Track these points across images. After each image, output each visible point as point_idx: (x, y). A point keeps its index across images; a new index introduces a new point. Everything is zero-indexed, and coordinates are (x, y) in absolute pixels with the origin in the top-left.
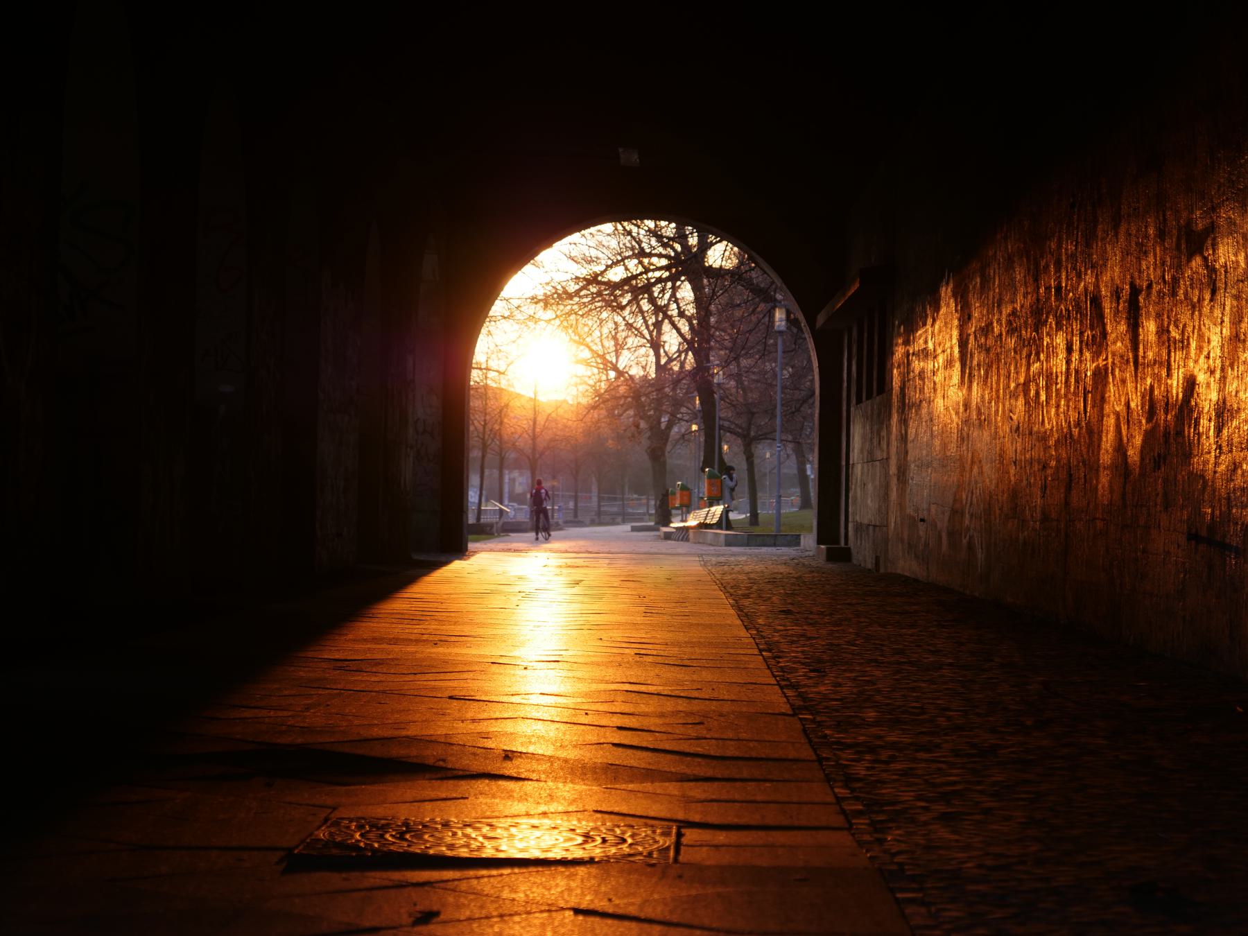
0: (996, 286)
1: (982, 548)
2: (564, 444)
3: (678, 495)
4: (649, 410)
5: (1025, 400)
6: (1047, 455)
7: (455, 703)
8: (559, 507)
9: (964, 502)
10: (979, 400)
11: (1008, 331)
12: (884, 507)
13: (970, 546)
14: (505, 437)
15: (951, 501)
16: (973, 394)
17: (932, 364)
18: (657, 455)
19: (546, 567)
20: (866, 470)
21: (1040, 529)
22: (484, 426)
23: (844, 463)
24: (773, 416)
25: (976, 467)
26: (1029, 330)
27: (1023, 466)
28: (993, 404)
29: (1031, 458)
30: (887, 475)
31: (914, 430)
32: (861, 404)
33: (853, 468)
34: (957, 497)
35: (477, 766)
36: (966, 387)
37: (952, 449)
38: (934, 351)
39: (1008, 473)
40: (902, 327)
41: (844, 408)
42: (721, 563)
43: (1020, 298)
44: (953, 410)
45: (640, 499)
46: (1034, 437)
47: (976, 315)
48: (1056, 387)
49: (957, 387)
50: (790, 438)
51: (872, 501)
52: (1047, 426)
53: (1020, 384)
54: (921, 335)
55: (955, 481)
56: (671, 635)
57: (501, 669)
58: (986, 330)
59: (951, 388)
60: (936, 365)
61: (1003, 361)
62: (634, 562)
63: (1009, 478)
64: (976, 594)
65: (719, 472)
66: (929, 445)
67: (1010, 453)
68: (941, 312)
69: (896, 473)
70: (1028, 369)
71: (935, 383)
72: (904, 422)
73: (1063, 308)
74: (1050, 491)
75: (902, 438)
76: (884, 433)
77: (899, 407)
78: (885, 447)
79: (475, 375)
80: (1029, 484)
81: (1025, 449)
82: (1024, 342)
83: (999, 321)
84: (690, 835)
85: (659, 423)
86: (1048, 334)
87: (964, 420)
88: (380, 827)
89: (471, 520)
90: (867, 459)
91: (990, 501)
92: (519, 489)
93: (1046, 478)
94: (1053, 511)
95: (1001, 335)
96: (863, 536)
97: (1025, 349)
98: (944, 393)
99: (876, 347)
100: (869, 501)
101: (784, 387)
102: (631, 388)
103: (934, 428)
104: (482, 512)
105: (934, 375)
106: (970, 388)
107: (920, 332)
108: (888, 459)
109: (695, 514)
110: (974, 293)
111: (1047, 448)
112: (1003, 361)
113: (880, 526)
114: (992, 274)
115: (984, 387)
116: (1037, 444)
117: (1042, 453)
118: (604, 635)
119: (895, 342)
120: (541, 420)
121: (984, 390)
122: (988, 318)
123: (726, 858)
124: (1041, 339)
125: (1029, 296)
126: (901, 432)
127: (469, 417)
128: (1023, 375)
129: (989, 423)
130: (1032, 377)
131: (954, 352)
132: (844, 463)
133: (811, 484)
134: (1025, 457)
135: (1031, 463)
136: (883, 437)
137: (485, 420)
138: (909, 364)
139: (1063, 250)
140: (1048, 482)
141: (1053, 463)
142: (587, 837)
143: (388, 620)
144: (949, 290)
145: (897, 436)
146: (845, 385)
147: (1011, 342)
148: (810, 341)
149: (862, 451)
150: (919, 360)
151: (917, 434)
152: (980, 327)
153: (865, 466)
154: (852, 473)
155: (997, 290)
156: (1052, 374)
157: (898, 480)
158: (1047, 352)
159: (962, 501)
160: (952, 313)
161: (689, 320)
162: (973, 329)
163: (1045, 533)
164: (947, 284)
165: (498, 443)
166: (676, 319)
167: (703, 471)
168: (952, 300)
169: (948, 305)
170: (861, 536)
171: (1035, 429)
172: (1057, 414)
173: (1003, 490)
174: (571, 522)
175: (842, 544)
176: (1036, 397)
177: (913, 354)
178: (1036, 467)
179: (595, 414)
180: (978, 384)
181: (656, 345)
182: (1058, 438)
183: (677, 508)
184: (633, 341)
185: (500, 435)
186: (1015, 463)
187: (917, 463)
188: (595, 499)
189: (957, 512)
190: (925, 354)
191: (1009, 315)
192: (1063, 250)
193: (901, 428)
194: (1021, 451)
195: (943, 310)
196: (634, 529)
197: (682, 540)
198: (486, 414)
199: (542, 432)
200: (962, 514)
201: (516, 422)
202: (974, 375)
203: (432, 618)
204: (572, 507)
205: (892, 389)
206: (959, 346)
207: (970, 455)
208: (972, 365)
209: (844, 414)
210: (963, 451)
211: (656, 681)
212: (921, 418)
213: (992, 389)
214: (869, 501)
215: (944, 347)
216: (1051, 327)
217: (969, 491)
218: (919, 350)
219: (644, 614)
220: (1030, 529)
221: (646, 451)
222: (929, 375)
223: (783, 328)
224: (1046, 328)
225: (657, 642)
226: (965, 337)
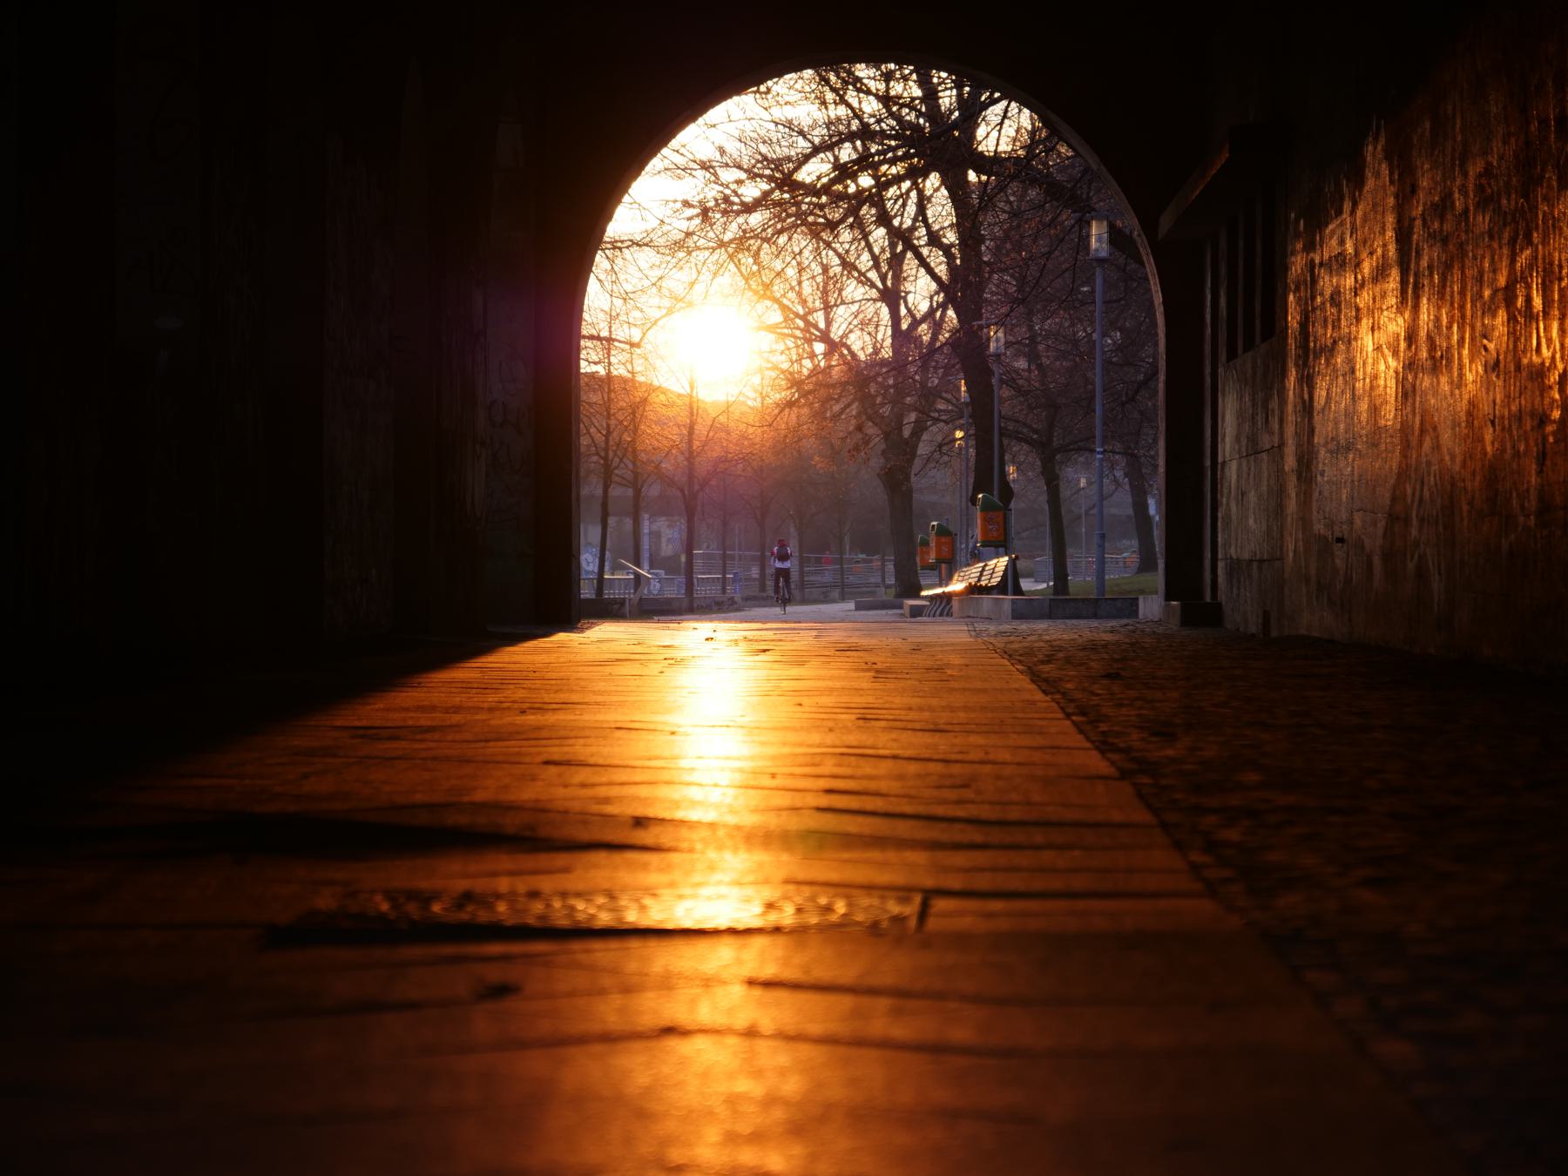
1: (1440, 574)
3: (933, 544)
4: (882, 405)
8: (735, 574)
9: (1409, 501)
11: (1479, 203)
14: (643, 456)
15: (1388, 502)
16: (1421, 317)
17: (1353, 276)
18: (897, 480)
20: (1245, 468)
22: (607, 436)
23: (1208, 463)
24: (1090, 410)
26: (1514, 196)
27: (1507, 425)
29: (1520, 411)
30: (1279, 472)
31: (1324, 393)
33: (1223, 468)
34: (1398, 492)
35: (584, 835)
36: (1409, 308)
37: (1389, 415)
39: (1482, 440)
40: (1302, 222)
41: (1208, 371)
42: (1006, 632)
43: (1497, 146)
45: (871, 561)
46: (1524, 374)
47: (1425, 184)
48: (1559, 286)
49: (1394, 310)
50: (1118, 447)
51: (1255, 522)
52: (1546, 352)
54: (1333, 232)
55: (1394, 467)
57: (633, 735)
58: (1442, 208)
59: (1385, 313)
60: (1359, 277)
61: (1471, 254)
65: (1001, 500)
66: (1350, 414)
67: (1486, 408)
68: (1367, 188)
70: (1513, 261)
71: (1358, 309)
72: (1308, 381)
76: (1274, 404)
77: (1298, 356)
78: (1277, 426)
79: (590, 362)
80: (1517, 455)
81: (1509, 397)
83: (1463, 190)
84: (940, 904)
85: (900, 427)
86: (1546, 199)
87: (1407, 362)
88: (426, 899)
89: (587, 592)
92: (667, 550)
93: (1545, 438)
94: (1557, 493)
95: (1466, 211)
96: (1242, 580)
97: (1508, 229)
98: (1373, 323)
100: (1251, 522)
102: (850, 369)
103: (1357, 385)
104: (606, 584)
105: (1356, 295)
106: (1416, 308)
107: (1331, 227)
108: (1282, 445)
109: (962, 574)
111: (1544, 389)
112: (1471, 254)
115: (1440, 303)
117: (1538, 399)
118: (805, 701)
119: (1290, 248)
120: (701, 430)
121: (1439, 308)
124: (1534, 208)
125: (1513, 140)
128: (1505, 272)
129: (1450, 361)
130: (1519, 274)
131: (1388, 250)
132: (1208, 463)
133: (1156, 533)
134: (1510, 410)
136: (1273, 411)
137: (608, 426)
138: (1314, 281)
140: (1548, 446)
142: (770, 906)
144: (1379, 147)
145: (1295, 407)
146: (1209, 330)
147: (1482, 222)
148: (1149, 260)
149: (1238, 439)
150: (1331, 273)
151: (1328, 397)
152: (1432, 204)
154: (1222, 478)
155: (1459, 138)
156: (1551, 264)
157: (1299, 478)
158: (1543, 230)
161: (946, 250)
162: (1420, 208)
164: (1376, 139)
166: (925, 251)
167: (973, 500)
168: (1384, 166)
169: (1377, 175)
170: (1239, 582)
171: (1525, 361)
174: (754, 598)
177: (1321, 264)
178: (1528, 424)
179: (791, 416)
180: (1429, 300)
181: (892, 297)
184: (853, 290)
185: (634, 451)
186: (1493, 423)
190: (1340, 263)
191: (1480, 176)
193: (1303, 390)
194: (1502, 401)
195: (1370, 184)
196: (858, 608)
200: (1407, 521)
201: (658, 436)
202: (1423, 285)
203: (521, 686)
204: (757, 576)
205: (1286, 328)
206: (1397, 240)
207: (1418, 419)
208: (1418, 269)
212: (1335, 370)
214: (1251, 522)
215: (1372, 245)
216: (1550, 187)
217: (1416, 480)
218: (1330, 257)
220: (1520, 528)
221: (878, 475)
222: (1348, 297)
223: (1104, 254)
224: (1542, 189)
225: (895, 706)
226: (1406, 223)
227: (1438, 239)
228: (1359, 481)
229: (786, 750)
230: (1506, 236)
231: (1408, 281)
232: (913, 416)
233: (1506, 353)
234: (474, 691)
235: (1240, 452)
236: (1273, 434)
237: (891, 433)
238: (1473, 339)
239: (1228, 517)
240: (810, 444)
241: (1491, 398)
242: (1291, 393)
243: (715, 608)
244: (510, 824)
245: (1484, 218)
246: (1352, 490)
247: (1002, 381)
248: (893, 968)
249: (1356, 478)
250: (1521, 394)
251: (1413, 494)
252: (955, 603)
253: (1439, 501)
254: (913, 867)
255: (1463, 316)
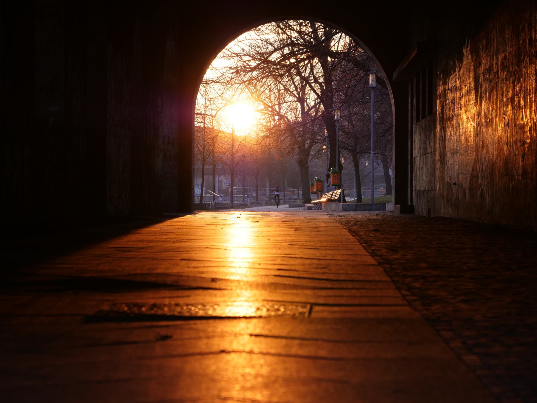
0: (495, 43)
1: (488, 195)
2: (249, 158)
3: (315, 185)
5: (512, 106)
6: (525, 136)
7: (184, 262)
9: (478, 170)
10: (486, 110)
11: (502, 68)
12: (432, 180)
13: (482, 195)
14: (216, 155)
15: (471, 171)
18: (303, 163)
19: (239, 218)
20: (422, 159)
21: (521, 179)
23: (409, 157)
24: (369, 139)
25: (484, 149)
28: (494, 111)
29: (516, 140)
30: (434, 161)
31: (449, 134)
32: (419, 122)
33: (414, 160)
34: (474, 168)
35: (194, 285)
36: (478, 104)
37: (471, 141)
38: (460, 86)
39: (503, 150)
40: (442, 75)
41: (409, 126)
43: (508, 48)
44: (471, 118)
45: (294, 191)
46: (518, 127)
48: (530, 97)
49: (473, 105)
52: (525, 120)
53: (509, 98)
54: (452, 78)
56: (309, 238)
57: (212, 250)
58: (489, 70)
59: (470, 106)
60: (461, 94)
61: (499, 86)
62: (289, 215)
63: (504, 152)
64: (486, 222)
66: (458, 141)
67: (504, 139)
68: (464, 63)
69: (439, 159)
70: (514, 88)
71: (461, 105)
72: (444, 129)
73: (533, 51)
74: (527, 157)
75: (442, 139)
76: (432, 137)
77: (440, 121)
79: (198, 122)
80: (515, 155)
82: (511, 74)
83: (497, 64)
84: (316, 308)
86: (525, 67)
89: (197, 201)
90: (423, 153)
91: (492, 167)
92: (224, 187)
93: (524, 149)
94: (529, 168)
95: (498, 71)
96: (421, 197)
97: (512, 77)
98: (466, 110)
99: (427, 89)
100: (424, 177)
101: (375, 123)
102: (287, 125)
105: (460, 100)
106: (481, 104)
107: (452, 76)
108: (435, 151)
109: (325, 195)
110: (482, 50)
111: (524, 132)
113: (430, 191)
114: (492, 37)
116: (519, 131)
117: (522, 136)
118: (271, 238)
120: (236, 146)
121: (489, 105)
122: (491, 63)
123: (338, 315)
124: (521, 70)
125: (514, 47)
126: (442, 135)
127: (194, 135)
128: (511, 92)
132: (409, 157)
134: (512, 139)
135: (516, 142)
136: (432, 139)
137: (204, 144)
138: (446, 95)
139: (533, 18)
141: (528, 141)
143: (147, 234)
146: (410, 112)
148: (389, 88)
149: (420, 149)
151: (451, 135)
152: (486, 69)
153: (422, 157)
154: (414, 163)
155: (495, 46)
156: (527, 90)
157: (440, 163)
159: (477, 170)
160: (470, 63)
161: (320, 84)
162: (482, 70)
163: (524, 181)
164: (467, 46)
165: (212, 158)
169: (468, 59)
170: (420, 198)
171: (518, 123)
172: (531, 112)
173: (500, 160)
174: (254, 203)
175: (409, 204)
176: (518, 104)
177: (448, 89)
179: (267, 141)
180: (485, 101)
181: (302, 100)
182: (531, 126)
183: (315, 193)
184: (289, 98)
185: (213, 153)
186: (507, 144)
187: (451, 152)
188: (268, 191)
189: (474, 177)
190: (455, 89)
191: (503, 59)
192: (533, 18)
194: (510, 136)
195: (465, 62)
197: (318, 209)
198: (204, 141)
199: (237, 151)
201: (221, 147)
202: (483, 97)
208: (481, 91)
209: (410, 129)
210: (477, 141)
211: (301, 254)
212: (453, 126)
213: (493, 103)
214: (424, 177)
216: (526, 63)
217: (481, 163)
218: (451, 87)
219: (294, 231)
220: (516, 180)
221: (297, 161)
223: (374, 85)
226: (477, 76)
227: (488, 81)
228: (461, 163)
229: (264, 255)
230: (511, 80)
231: (478, 95)
232: (309, 141)
233: (511, 120)
234: (158, 235)
235: (420, 154)
236: (432, 147)
237: (301, 147)
238: (500, 115)
239: (416, 176)
240: (274, 151)
241: (506, 135)
242: (438, 133)
243: (241, 207)
244: (169, 280)
245: (504, 74)
246: (459, 166)
247: (339, 129)
248: (300, 330)
249: (460, 163)
250: (516, 134)
251: (480, 168)
252: (323, 205)
253: (488, 171)
254: (307, 296)
255: (497, 107)
